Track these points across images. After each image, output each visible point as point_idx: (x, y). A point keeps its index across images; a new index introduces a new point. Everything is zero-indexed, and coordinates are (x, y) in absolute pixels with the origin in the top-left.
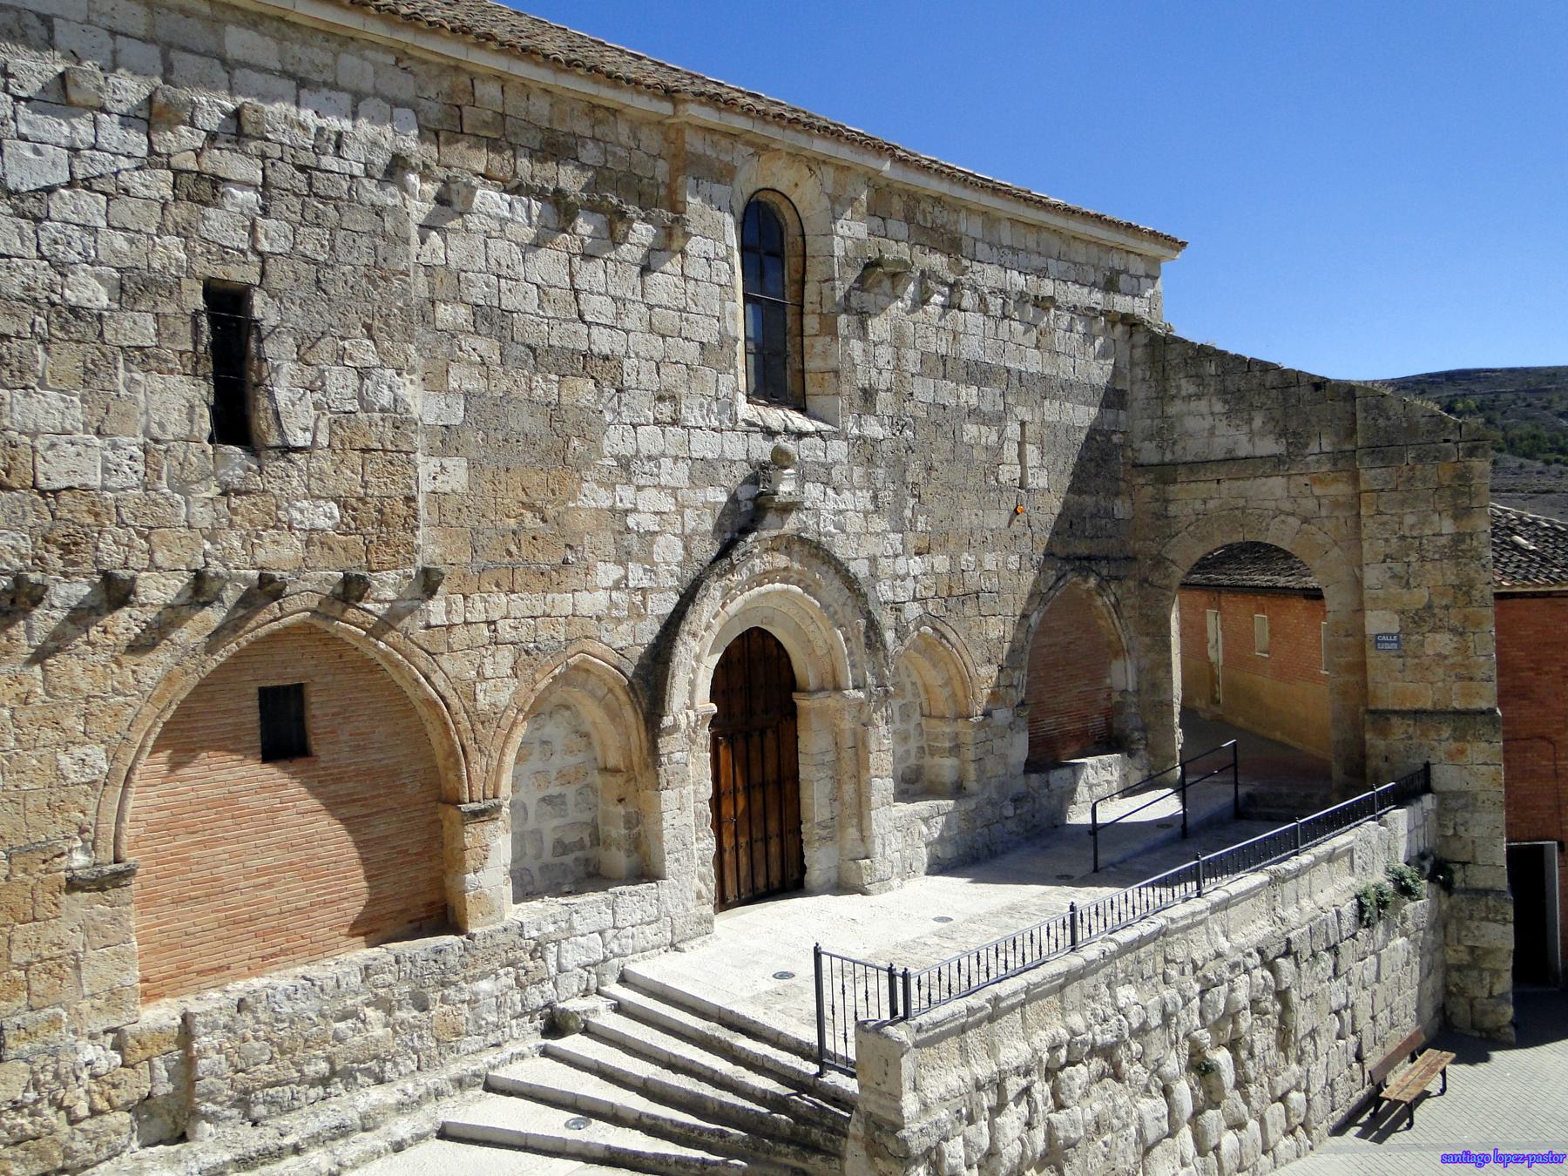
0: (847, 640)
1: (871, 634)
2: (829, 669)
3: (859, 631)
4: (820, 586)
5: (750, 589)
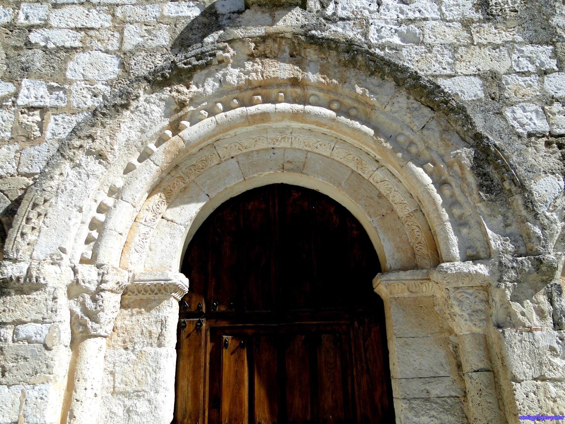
0: (440, 184)
1: (489, 169)
2: (422, 237)
3: (461, 167)
4: (373, 107)
5: (227, 108)
